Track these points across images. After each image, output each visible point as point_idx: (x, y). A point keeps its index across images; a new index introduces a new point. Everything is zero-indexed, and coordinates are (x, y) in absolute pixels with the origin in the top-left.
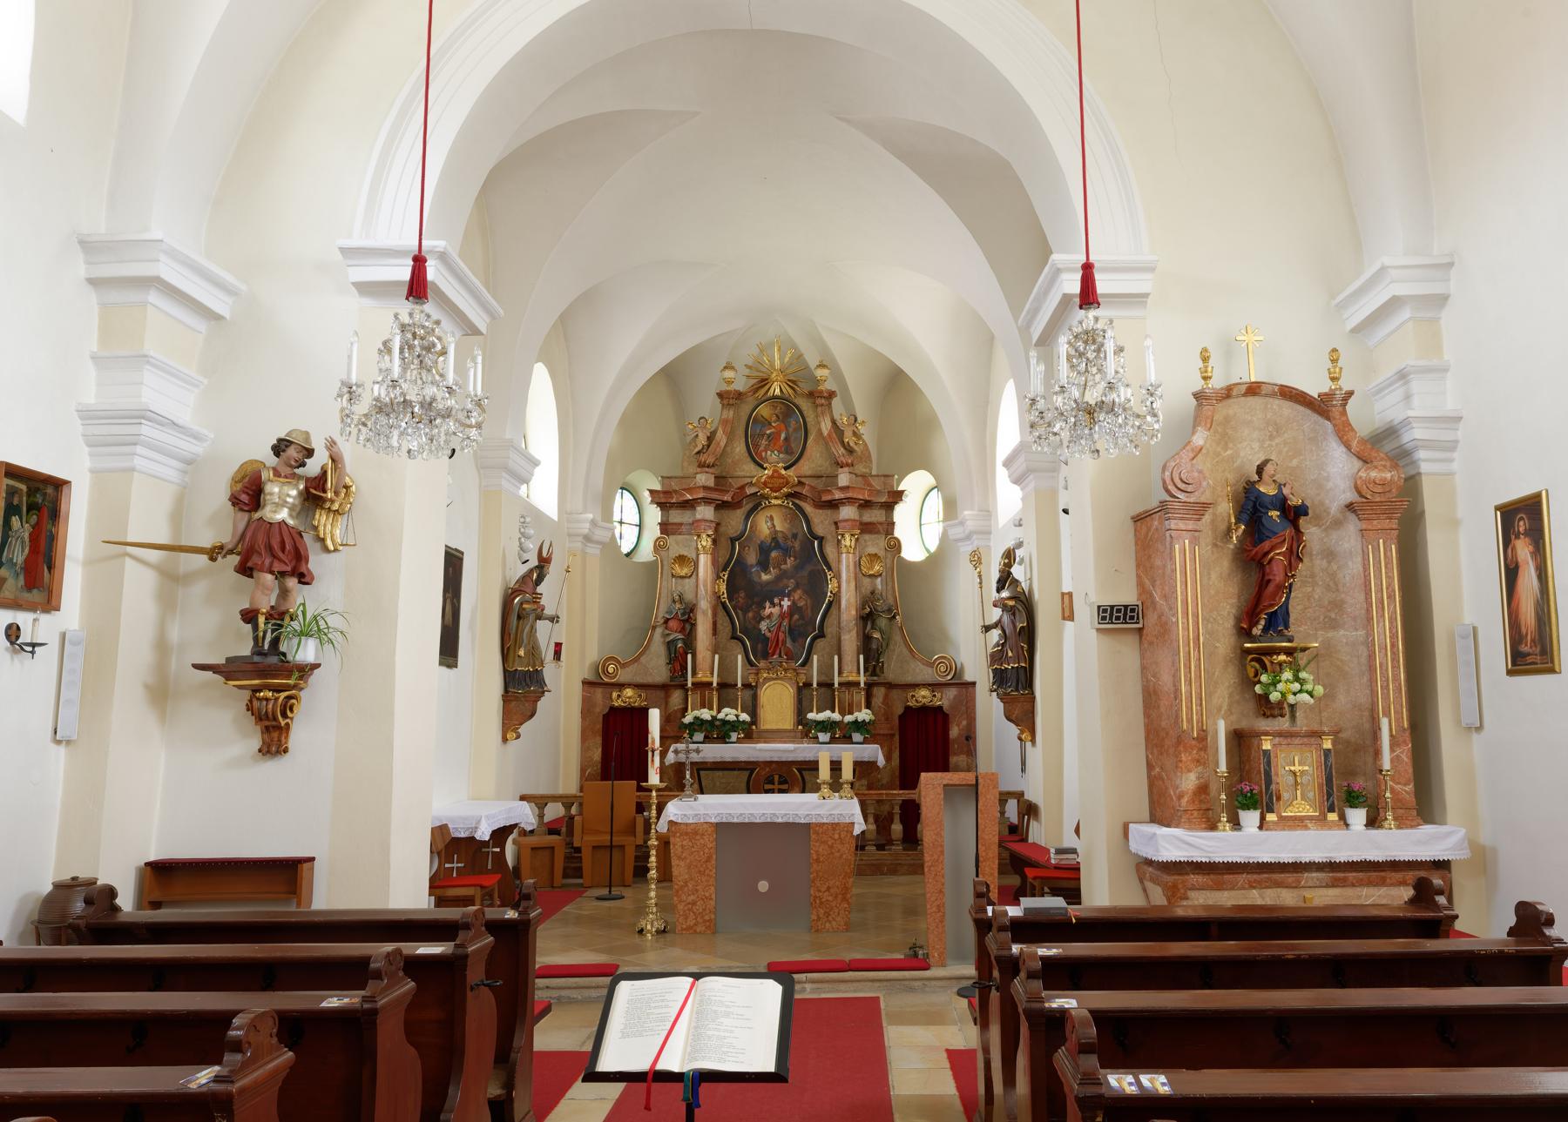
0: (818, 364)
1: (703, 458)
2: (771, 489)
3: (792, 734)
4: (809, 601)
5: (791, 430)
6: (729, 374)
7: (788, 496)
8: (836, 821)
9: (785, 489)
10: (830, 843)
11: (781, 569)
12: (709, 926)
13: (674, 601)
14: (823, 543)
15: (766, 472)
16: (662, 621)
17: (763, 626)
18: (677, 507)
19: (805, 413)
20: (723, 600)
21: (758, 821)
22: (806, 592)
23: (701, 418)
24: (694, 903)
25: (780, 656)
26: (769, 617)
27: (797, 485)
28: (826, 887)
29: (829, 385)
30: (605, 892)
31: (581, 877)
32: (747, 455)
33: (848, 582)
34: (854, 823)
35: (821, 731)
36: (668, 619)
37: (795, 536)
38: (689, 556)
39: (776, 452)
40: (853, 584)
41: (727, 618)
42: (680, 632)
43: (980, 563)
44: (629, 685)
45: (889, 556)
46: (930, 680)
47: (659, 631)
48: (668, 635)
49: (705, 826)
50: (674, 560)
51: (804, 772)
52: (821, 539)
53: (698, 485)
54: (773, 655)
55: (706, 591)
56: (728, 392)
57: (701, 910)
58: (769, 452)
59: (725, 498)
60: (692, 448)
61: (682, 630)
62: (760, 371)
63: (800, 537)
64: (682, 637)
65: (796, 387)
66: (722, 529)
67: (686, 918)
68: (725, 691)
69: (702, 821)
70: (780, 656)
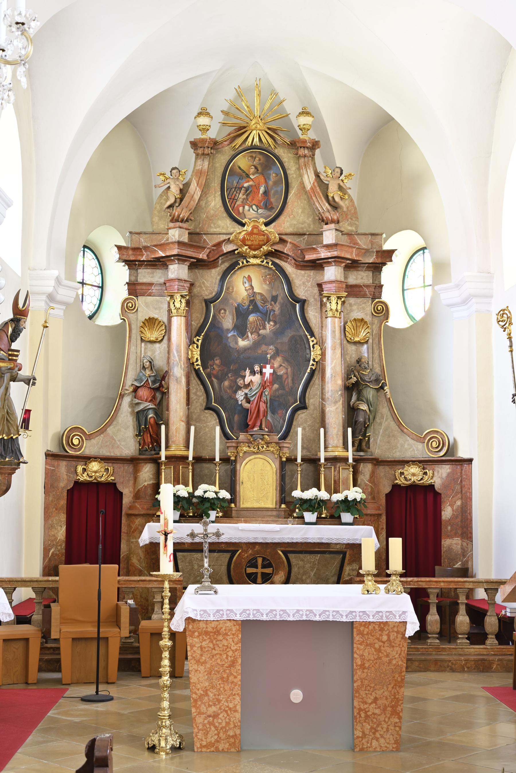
0: (301, 111)
1: (176, 212)
2: (250, 247)
3: (274, 513)
4: (289, 370)
5: (271, 183)
6: (203, 121)
7: (269, 254)
8: (385, 620)
9: (265, 248)
10: (377, 646)
11: (259, 335)
12: (234, 743)
13: (144, 368)
14: (305, 307)
15: (245, 228)
16: (131, 389)
17: (240, 396)
18: (146, 265)
19: (286, 165)
20: (197, 367)
21: (291, 619)
22: (286, 360)
23: (173, 169)
24: (215, 716)
25: (261, 428)
26: (247, 386)
27: (277, 243)
28: (372, 698)
29: (311, 135)
30: (90, 690)
31: (59, 670)
32: (223, 209)
33: (334, 349)
34: (406, 622)
35: (307, 510)
36: (138, 387)
37: (274, 299)
38: (160, 319)
39: (254, 207)
40: (338, 351)
41: (201, 387)
42: (151, 401)
43: (511, 324)
44: (95, 458)
45: (376, 322)
46: (420, 456)
47: (127, 400)
48: (138, 404)
49: (229, 624)
50: (143, 323)
51: (290, 555)
52: (303, 303)
53: (170, 241)
54: (253, 428)
55: (180, 356)
56: (203, 141)
57: (224, 724)
58: (247, 207)
59: (200, 257)
60: (163, 201)
61: (153, 400)
62: (237, 118)
63: (280, 298)
64: (154, 406)
65: (276, 136)
66: (196, 290)
67: (206, 734)
68: (198, 466)
69: (225, 618)
70: (261, 428)
